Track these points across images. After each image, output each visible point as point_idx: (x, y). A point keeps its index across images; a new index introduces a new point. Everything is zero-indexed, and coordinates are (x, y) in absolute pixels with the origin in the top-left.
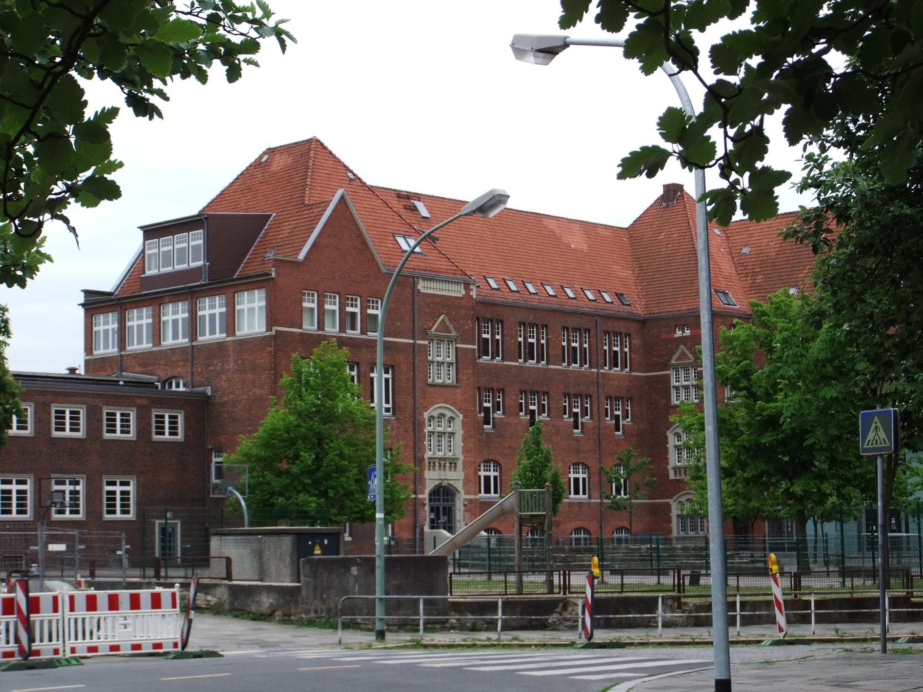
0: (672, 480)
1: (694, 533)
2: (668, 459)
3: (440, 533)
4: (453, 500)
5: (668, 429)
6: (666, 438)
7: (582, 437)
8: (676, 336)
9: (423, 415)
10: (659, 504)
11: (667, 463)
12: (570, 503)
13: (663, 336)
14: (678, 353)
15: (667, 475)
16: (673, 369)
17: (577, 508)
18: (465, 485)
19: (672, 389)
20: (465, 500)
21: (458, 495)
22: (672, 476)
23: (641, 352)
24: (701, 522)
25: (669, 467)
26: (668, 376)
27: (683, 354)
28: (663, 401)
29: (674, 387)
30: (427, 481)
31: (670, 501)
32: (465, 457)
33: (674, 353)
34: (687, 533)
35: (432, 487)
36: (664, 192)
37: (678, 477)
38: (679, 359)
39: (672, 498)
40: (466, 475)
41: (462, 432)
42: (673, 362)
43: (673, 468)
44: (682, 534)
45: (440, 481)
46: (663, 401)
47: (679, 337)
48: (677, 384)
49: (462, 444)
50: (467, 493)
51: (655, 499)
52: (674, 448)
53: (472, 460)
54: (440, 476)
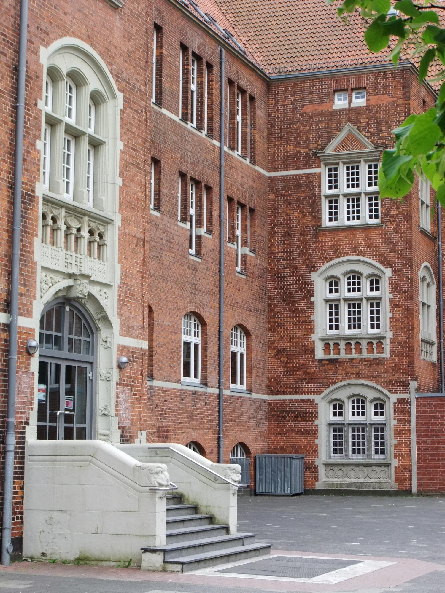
0: (321, 361)
1: (361, 456)
2: (312, 322)
3: (97, 449)
4: (90, 348)
5: (315, 268)
6: (311, 285)
7: (200, 264)
8: (334, 107)
9: (36, 53)
10: (293, 403)
11: (312, 330)
12: (182, 392)
13: (309, 108)
14: (341, 136)
15: (312, 352)
16: (326, 165)
17: (189, 401)
18: (122, 303)
19: (323, 198)
20: (122, 349)
21: (103, 333)
22: (320, 353)
23: (265, 134)
24: (376, 437)
25: (315, 337)
26: (317, 177)
27: (350, 137)
28: (305, 221)
29: (326, 197)
30: (40, 275)
31: (317, 398)
32: (124, 220)
33: (333, 137)
34: (347, 456)
35: (48, 296)
36: (40, 64)
37: (332, 356)
38: (342, 145)
39: (320, 392)
40: (125, 275)
41: (120, 145)
42: (329, 151)
43: (322, 340)
44: (337, 458)
45: (69, 282)
46: (305, 221)
47: (343, 110)
48: (333, 192)
49: (120, 181)
50: (127, 331)
51: (284, 393)
52: (324, 302)
53: (139, 235)
54: (68, 264)
